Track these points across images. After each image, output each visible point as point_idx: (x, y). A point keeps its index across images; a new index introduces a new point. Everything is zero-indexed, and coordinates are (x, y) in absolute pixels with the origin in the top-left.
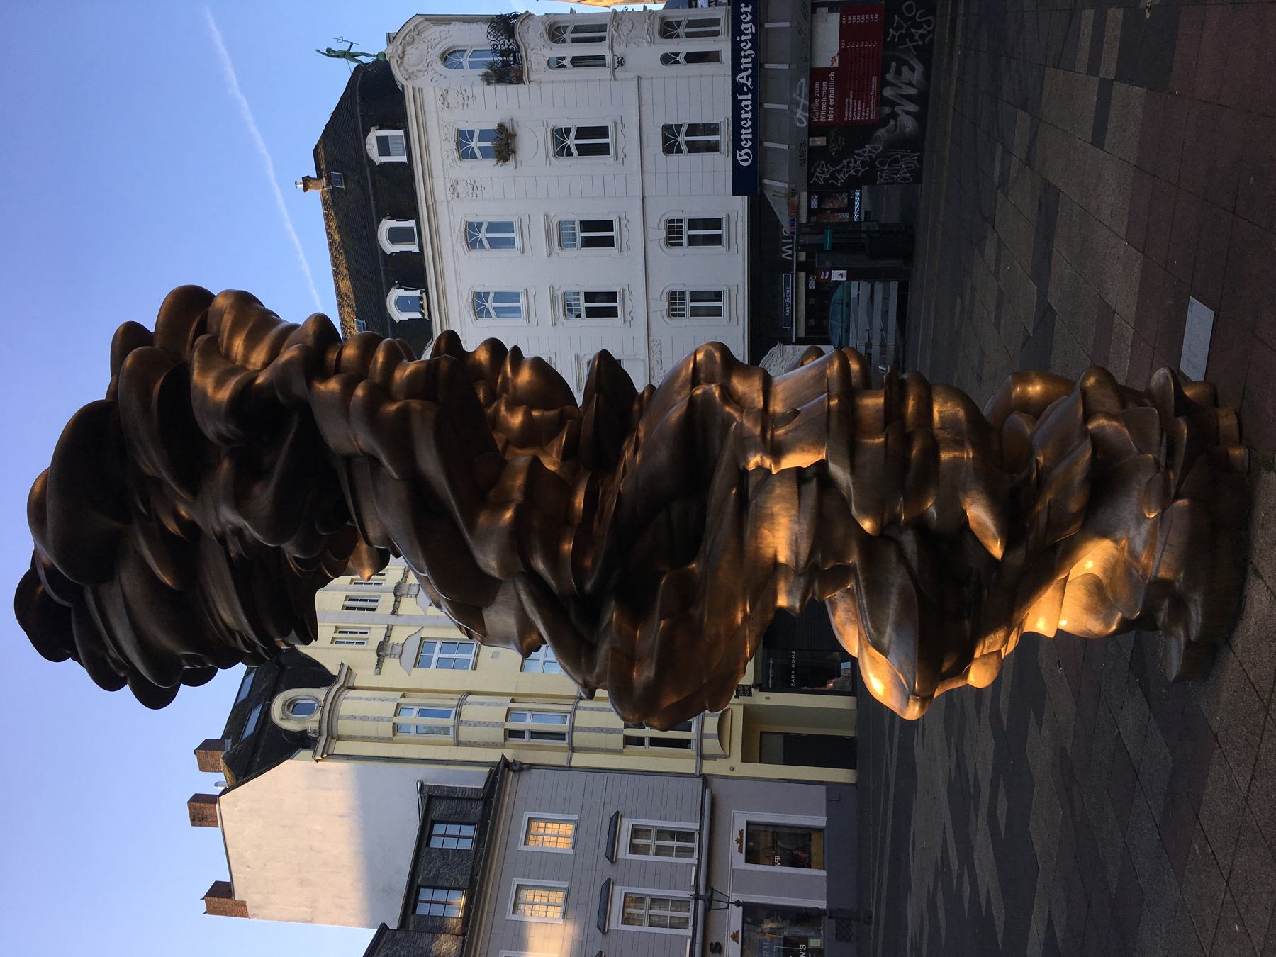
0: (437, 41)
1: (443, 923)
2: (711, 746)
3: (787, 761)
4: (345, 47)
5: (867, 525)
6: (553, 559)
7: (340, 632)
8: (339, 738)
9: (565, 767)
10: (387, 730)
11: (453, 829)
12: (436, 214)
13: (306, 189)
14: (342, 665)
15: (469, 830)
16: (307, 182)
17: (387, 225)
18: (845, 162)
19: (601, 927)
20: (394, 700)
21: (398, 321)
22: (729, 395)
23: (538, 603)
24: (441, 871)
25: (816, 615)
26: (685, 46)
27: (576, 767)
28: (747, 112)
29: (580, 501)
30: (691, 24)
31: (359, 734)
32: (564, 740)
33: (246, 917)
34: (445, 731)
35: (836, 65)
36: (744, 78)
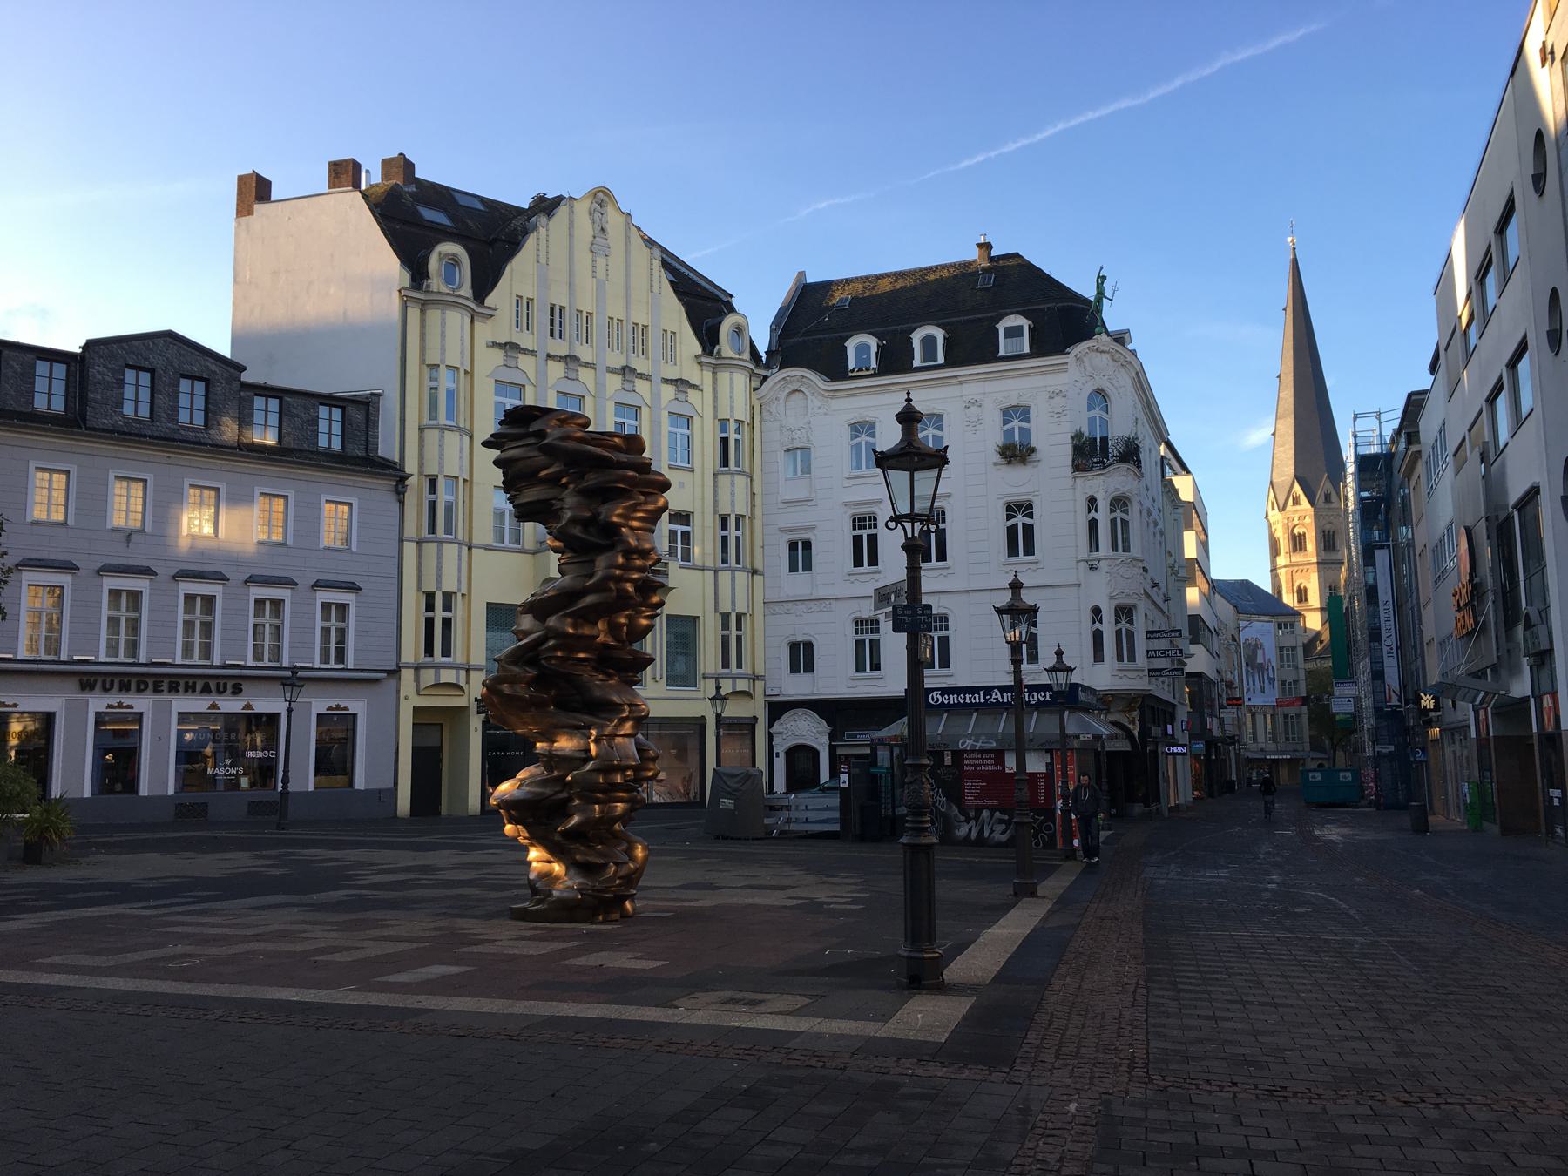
0: (1116, 384)
1: (248, 424)
2: (428, 677)
3: (415, 750)
4: (1108, 293)
5: (569, 778)
6: (555, 648)
7: (528, 303)
8: (423, 312)
9: (402, 536)
10: (432, 358)
11: (337, 428)
12: (949, 385)
13: (979, 245)
14: (495, 309)
15: (337, 444)
16: (986, 247)
17: (939, 334)
18: (932, 781)
19: (251, 579)
20: (462, 364)
21: (846, 344)
22: (623, 721)
23: (535, 640)
24: (296, 419)
25: (530, 758)
26: (1108, 628)
27: (402, 545)
28: (970, 699)
29: (581, 655)
30: (1131, 635)
31: (428, 330)
32: (429, 533)
33: (237, 214)
34: (433, 416)
35: (1007, 771)
36: (996, 695)
